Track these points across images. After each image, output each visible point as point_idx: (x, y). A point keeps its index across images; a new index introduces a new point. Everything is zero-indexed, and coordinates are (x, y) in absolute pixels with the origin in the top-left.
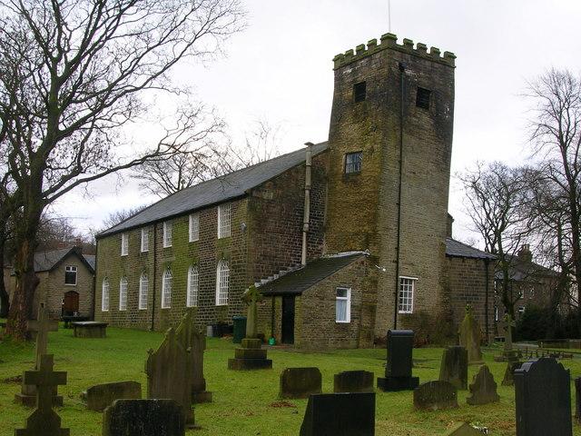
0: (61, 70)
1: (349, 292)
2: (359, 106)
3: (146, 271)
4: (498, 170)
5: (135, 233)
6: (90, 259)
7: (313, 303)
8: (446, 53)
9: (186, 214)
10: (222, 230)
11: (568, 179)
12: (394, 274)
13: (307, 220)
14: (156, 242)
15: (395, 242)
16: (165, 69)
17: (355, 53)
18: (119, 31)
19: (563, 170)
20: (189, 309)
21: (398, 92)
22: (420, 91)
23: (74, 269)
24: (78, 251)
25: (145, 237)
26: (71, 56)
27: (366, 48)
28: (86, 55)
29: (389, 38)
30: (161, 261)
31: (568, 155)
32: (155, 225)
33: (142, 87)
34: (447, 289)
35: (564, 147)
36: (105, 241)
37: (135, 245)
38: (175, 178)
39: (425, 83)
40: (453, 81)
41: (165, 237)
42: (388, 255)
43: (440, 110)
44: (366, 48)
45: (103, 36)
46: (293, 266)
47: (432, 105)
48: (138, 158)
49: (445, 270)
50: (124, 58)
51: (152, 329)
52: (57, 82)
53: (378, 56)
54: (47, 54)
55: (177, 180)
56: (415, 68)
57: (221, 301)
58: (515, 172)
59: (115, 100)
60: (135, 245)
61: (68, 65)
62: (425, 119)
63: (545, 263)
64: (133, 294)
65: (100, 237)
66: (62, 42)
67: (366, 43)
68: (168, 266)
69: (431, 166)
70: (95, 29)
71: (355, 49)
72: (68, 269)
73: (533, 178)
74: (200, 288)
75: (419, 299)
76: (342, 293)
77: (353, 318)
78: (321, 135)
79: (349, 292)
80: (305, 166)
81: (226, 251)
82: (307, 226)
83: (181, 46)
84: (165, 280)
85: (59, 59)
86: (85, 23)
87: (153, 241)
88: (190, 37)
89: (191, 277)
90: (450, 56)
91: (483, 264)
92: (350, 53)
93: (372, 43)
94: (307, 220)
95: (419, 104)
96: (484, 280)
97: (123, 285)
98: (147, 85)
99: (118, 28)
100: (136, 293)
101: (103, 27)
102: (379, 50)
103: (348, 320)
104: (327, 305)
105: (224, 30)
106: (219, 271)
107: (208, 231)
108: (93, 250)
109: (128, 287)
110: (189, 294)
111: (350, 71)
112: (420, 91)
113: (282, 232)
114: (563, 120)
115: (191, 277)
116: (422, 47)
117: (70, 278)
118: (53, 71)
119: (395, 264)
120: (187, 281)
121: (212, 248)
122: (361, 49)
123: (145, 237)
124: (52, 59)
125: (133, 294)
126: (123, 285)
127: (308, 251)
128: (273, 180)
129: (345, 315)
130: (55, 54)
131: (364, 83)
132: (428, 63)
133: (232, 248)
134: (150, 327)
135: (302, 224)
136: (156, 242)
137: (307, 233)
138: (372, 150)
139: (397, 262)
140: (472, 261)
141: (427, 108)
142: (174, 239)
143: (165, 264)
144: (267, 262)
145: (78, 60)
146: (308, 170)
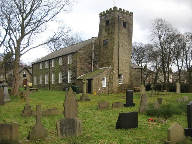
0: (24, 15)
1: (106, 78)
2: (107, 27)
3: (47, 73)
4: (141, 45)
5: (44, 63)
6: (30, 70)
7: (97, 81)
8: (130, 12)
9: (59, 57)
10: (69, 62)
11: (161, 47)
12: (118, 73)
13: (93, 59)
14: (50, 65)
15: (117, 64)
16: (55, 15)
17: (106, 12)
18: (41, 5)
19: (159, 44)
20: (60, 84)
21: (115, 22)
22: (124, 22)
23: (25, 73)
24: (26, 68)
25: (46, 64)
26: (27, 12)
27: (109, 11)
28: (32, 11)
29: (115, 8)
30: (51, 70)
31: (161, 40)
32: (49, 61)
33: (49, 21)
34: (131, 78)
35: (160, 38)
36: (35, 65)
37: (44, 66)
38: (53, 48)
39: (125, 21)
40: (132, 20)
41: (52, 64)
42: (116, 68)
43: (129, 28)
44: (109, 11)
45: (37, 6)
46: (89, 71)
47: (127, 27)
48: (48, 41)
49: (131, 72)
50: (42, 12)
51: (49, 89)
52: (24, 19)
53: (112, 13)
54: (20, 11)
55: (54, 48)
56: (122, 16)
57: (69, 81)
58: (145, 46)
59: (41, 24)
60: (44, 66)
61: (26, 15)
62: (125, 30)
63: (152, 69)
64: (43, 80)
65: (34, 64)
66: (25, 8)
67: (109, 9)
68: (53, 72)
69: (127, 43)
70: (34, 4)
71: (105, 11)
72: (24, 73)
73: (150, 47)
74: (42, 82)
75: (124, 80)
76: (104, 79)
77: (107, 85)
78: (96, 35)
79: (106, 78)
80: (92, 44)
81: (71, 68)
82: (93, 60)
83: (59, 9)
84: (53, 76)
85: (23, 13)
86: (31, 2)
87: (49, 65)
88: (62, 6)
89: (60, 75)
90: (131, 13)
91: (140, 70)
92: (104, 12)
93: (110, 9)
94: (93, 59)
95: (124, 26)
96: (141, 74)
97: (40, 77)
98: (50, 20)
99: (42, 3)
100: (44, 79)
101: (37, 3)
102: (113, 11)
103: (106, 86)
104: (100, 81)
105: (71, 4)
106: (68, 73)
107: (65, 62)
108: (29, 67)
109: (42, 78)
110: (60, 80)
111: (104, 17)
112: (124, 22)
113: (86, 62)
114: (160, 31)
115: (60, 75)
116: (124, 10)
117: (24, 76)
118: (22, 16)
119: (118, 71)
120: (68, 75)
121: (66, 67)
122: (107, 11)
123: (46, 64)
124: (22, 13)
125: (43, 80)
126: (40, 77)
127: (93, 67)
128: (83, 48)
129: (105, 84)
130: (23, 11)
131: (108, 21)
132: (126, 15)
133: (72, 67)
134: (49, 89)
135: (92, 60)
136: (50, 65)
137: (93, 62)
138: (111, 39)
139: (118, 70)
140: (138, 69)
141: (126, 27)
142: (55, 64)
143: (53, 72)
144: (82, 70)
145: (29, 13)
146: (93, 45)
